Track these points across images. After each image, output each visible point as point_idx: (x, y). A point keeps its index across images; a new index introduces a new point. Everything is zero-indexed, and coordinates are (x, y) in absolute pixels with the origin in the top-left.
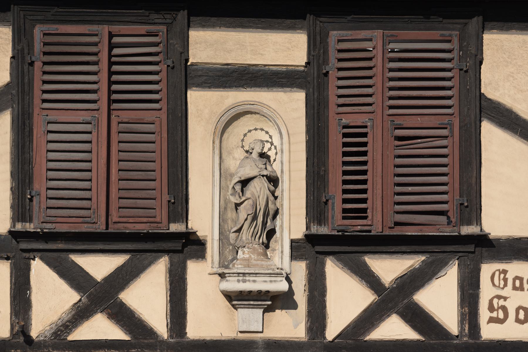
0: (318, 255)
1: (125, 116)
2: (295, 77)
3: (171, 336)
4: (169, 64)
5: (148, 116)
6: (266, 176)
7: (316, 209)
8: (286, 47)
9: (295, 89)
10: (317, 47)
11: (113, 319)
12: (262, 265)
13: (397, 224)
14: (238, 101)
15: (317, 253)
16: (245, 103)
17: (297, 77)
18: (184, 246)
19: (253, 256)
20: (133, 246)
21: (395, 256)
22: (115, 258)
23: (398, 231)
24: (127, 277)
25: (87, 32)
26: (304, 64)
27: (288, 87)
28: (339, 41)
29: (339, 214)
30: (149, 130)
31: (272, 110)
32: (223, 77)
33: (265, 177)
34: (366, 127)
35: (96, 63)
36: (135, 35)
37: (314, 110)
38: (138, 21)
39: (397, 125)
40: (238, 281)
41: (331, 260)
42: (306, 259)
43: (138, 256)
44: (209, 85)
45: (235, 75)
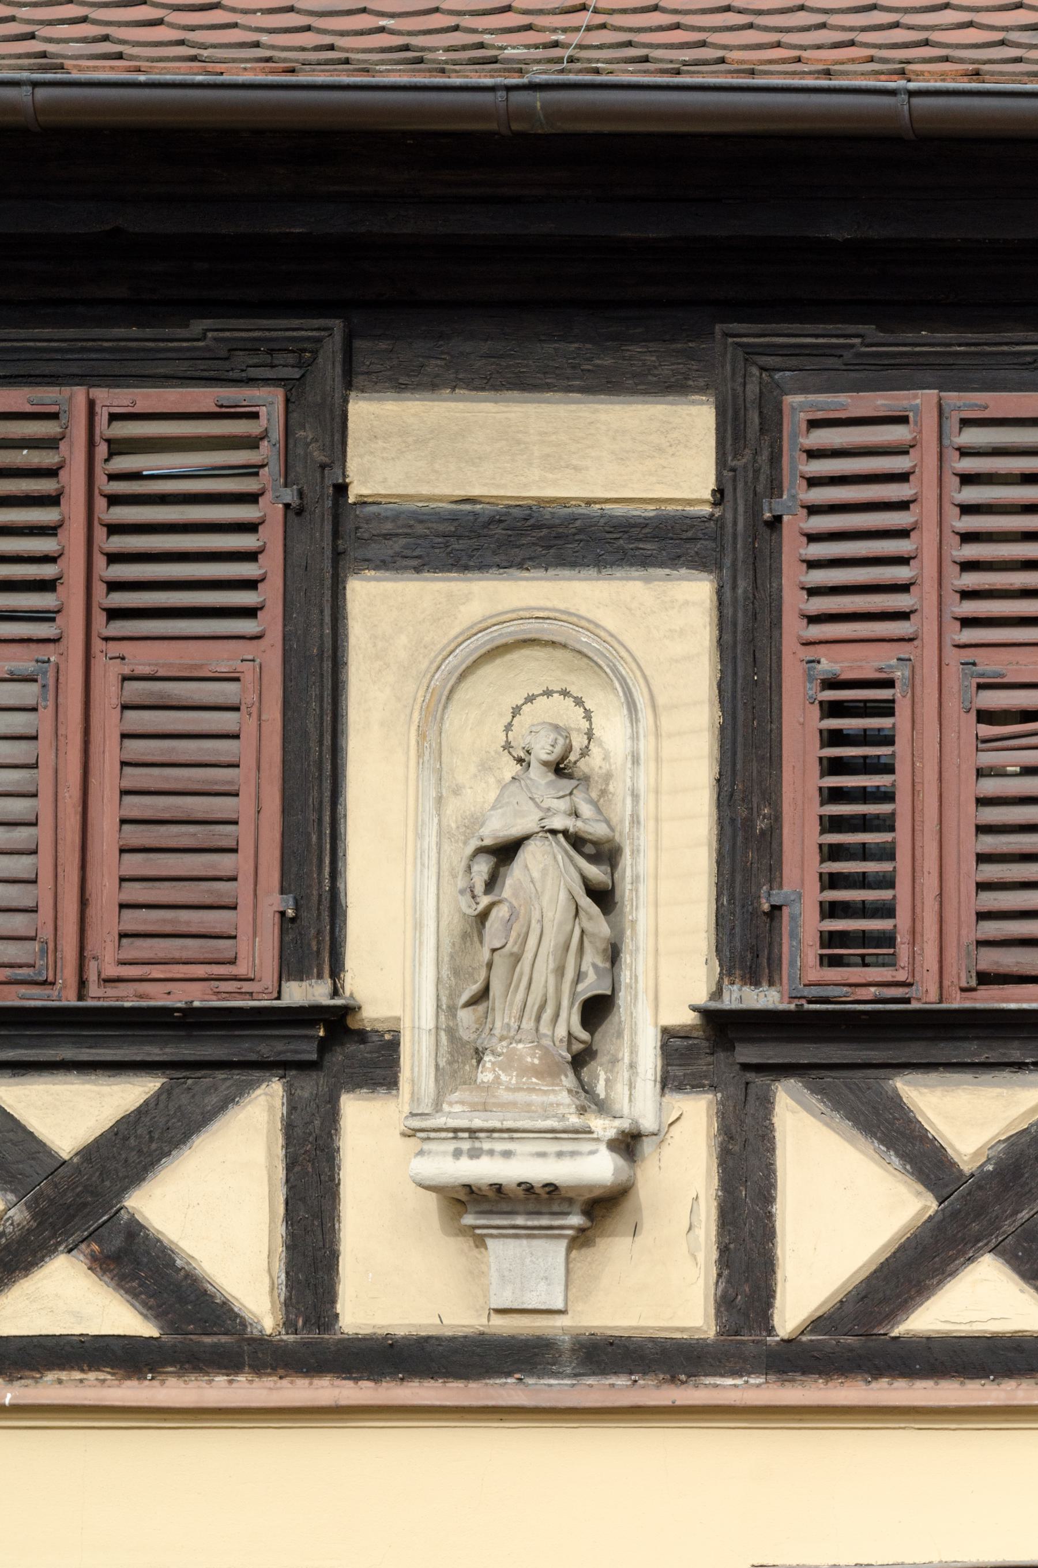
0: (750, 1076)
1: (143, 658)
2: (685, 535)
3: (289, 1325)
4: (288, 499)
5: (221, 658)
6: (565, 833)
7: (746, 936)
8: (655, 449)
9: (683, 571)
10: (747, 446)
11: (104, 1271)
12: (529, 1105)
13: (985, 978)
14: (500, 608)
15: (746, 1067)
16: (522, 614)
17: (690, 534)
18: (324, 1046)
19: (504, 1078)
20: (167, 1050)
21: (987, 1077)
22: (115, 1088)
23: (127, 997)
24: (154, 1146)
25: (28, 408)
26: (707, 495)
27: (662, 565)
28: (814, 424)
29: (812, 951)
30: (221, 701)
31: (602, 634)
32: (460, 537)
33: (560, 836)
34: (889, 684)
35: (53, 500)
36: (184, 427)
37: (735, 632)
38: (198, 374)
39: (982, 675)
40: (457, 1154)
41: (788, 1092)
42: (714, 1087)
43: (190, 1081)
44: (415, 563)
45: (498, 531)
